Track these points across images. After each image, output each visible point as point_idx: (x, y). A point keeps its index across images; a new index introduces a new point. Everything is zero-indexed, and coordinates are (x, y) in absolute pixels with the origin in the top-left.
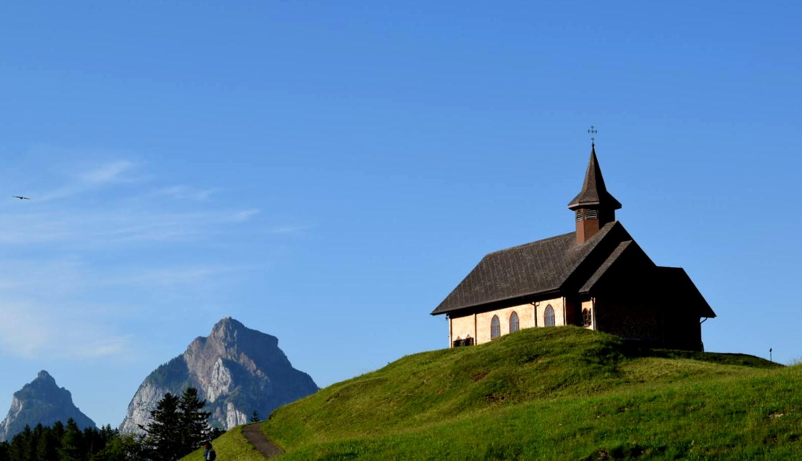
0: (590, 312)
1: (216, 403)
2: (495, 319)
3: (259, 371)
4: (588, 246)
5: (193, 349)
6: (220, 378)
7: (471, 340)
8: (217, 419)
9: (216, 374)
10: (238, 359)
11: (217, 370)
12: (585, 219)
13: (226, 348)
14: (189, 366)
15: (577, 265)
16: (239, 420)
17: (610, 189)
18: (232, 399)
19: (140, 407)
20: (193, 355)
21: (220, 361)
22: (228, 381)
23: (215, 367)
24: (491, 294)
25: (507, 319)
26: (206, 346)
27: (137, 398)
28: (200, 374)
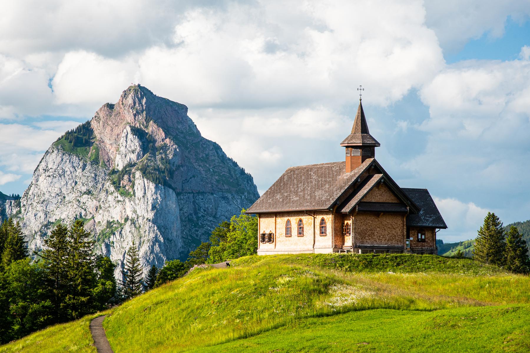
0: (350, 226)
1: (124, 171)
2: (288, 222)
3: (168, 140)
4: (352, 177)
5: (101, 115)
6: (128, 146)
7: (272, 235)
8: (124, 187)
9: (125, 141)
10: (147, 127)
11: (125, 138)
12: (352, 155)
13: (135, 115)
14: (96, 133)
15: (343, 191)
16: (147, 188)
17: (373, 131)
18: (140, 168)
19: (46, 173)
20: (101, 122)
21: (129, 129)
22: (136, 149)
23: (124, 135)
24: (286, 203)
25: (296, 223)
26: (114, 114)
27: (43, 164)
28: (107, 142)
